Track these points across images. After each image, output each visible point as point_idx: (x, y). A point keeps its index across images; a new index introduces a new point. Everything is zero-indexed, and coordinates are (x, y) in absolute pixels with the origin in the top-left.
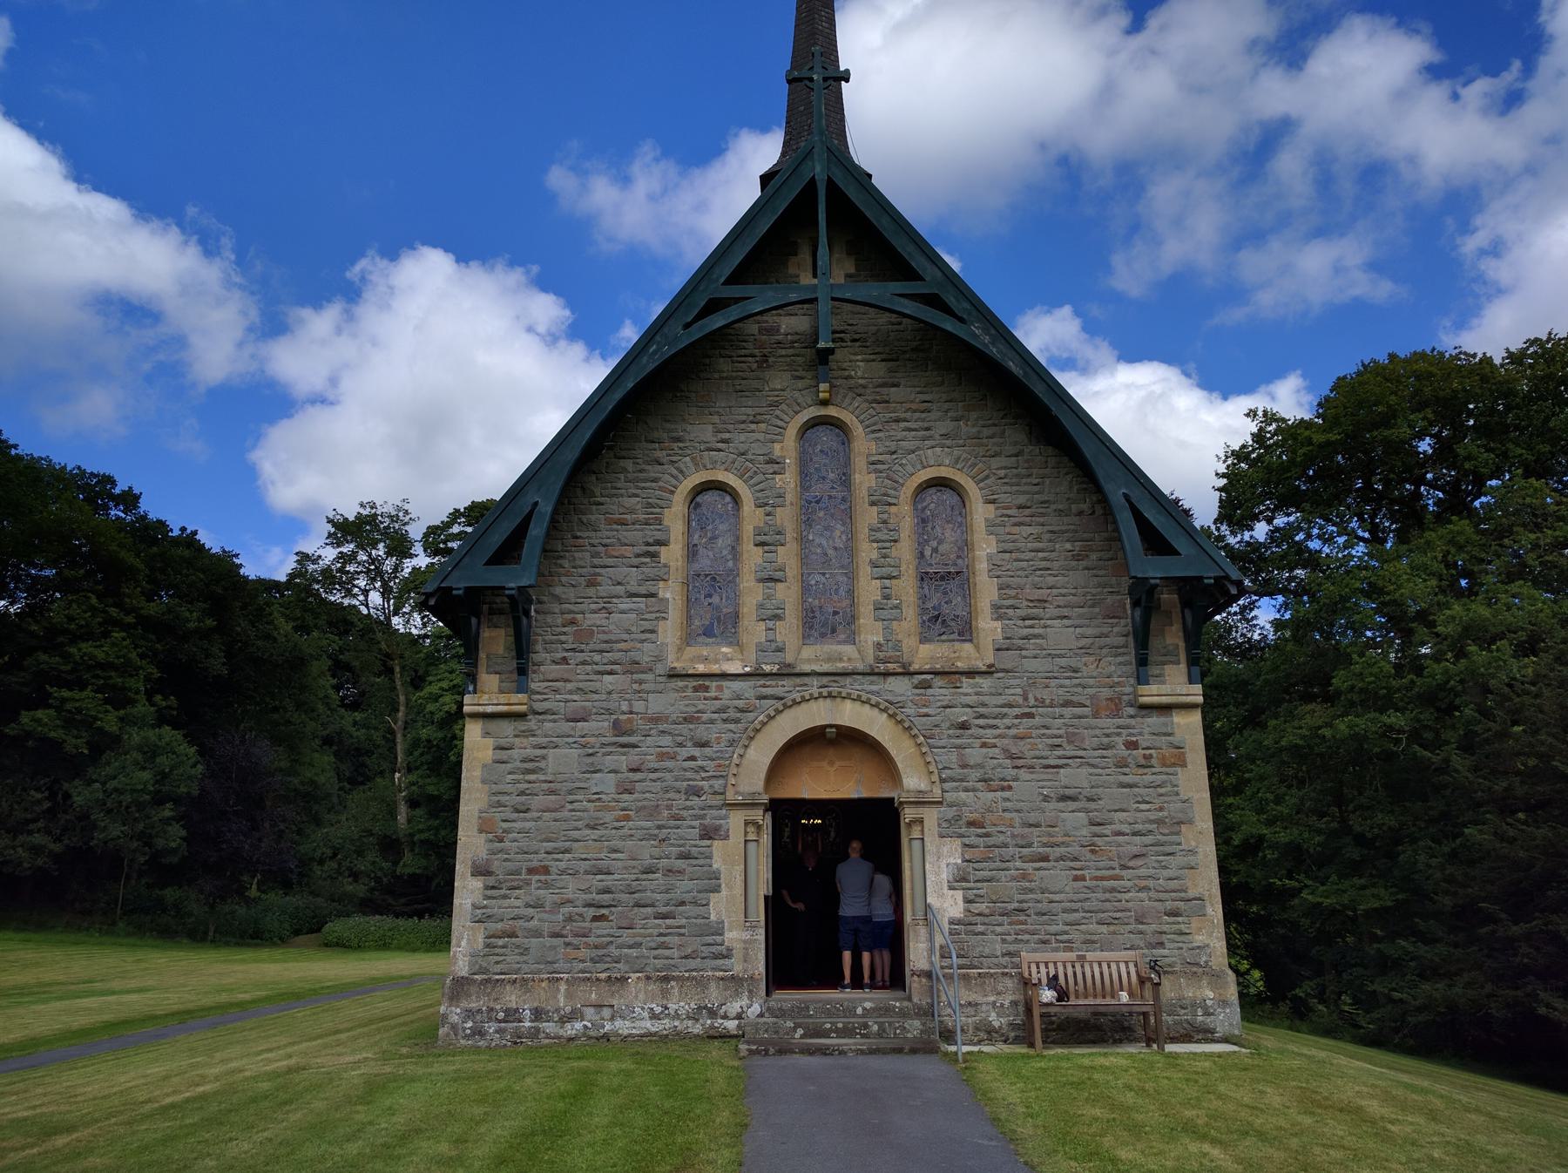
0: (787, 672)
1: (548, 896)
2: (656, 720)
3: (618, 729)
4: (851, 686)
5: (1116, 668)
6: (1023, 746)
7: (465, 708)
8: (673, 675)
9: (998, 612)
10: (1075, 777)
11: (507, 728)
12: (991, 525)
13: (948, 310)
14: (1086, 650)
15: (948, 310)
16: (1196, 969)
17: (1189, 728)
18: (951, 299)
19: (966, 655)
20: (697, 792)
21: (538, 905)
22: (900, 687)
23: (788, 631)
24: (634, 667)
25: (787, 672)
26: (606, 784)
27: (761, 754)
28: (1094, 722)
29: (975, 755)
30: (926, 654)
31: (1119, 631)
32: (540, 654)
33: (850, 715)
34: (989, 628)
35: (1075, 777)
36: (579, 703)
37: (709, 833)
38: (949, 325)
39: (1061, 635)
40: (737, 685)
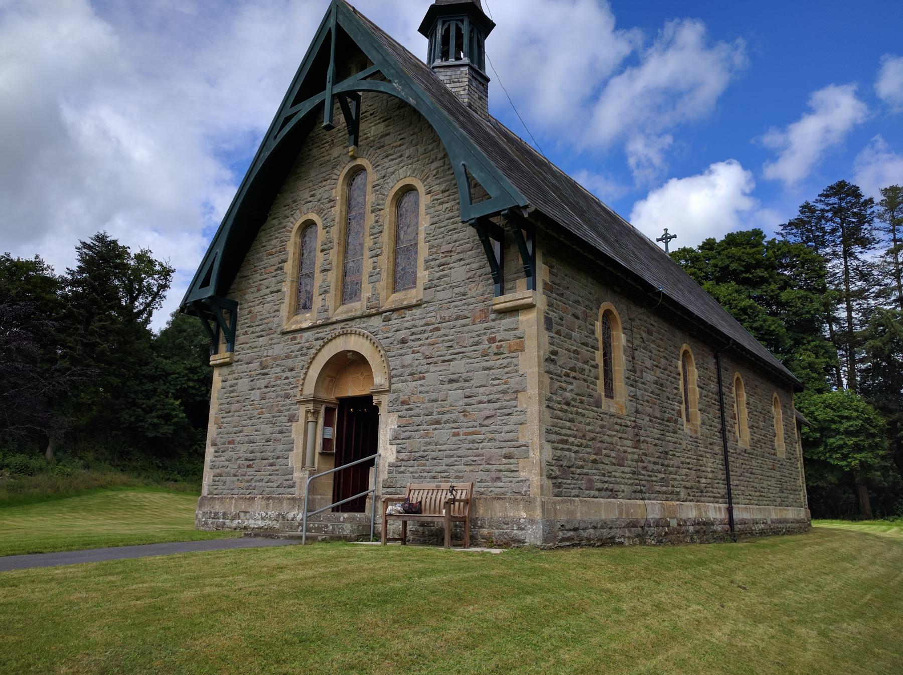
10: (459, 366)
23: (331, 299)
34: (423, 276)
35: (459, 366)
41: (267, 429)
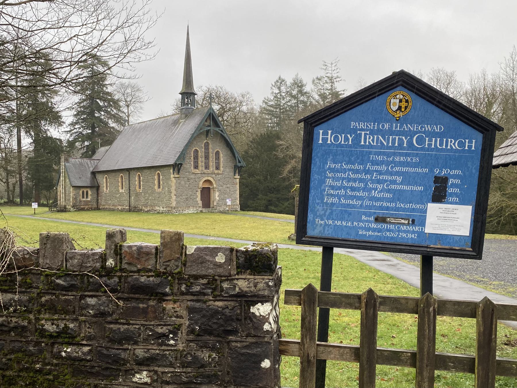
0: (204, 173)
1: (182, 198)
2: (191, 178)
3: (188, 179)
4: (210, 175)
5: (232, 174)
6: (224, 182)
7: (494, 160)
8: (193, 173)
9: (223, 167)
10: (228, 185)
11: (177, 179)
12: (119, 329)
13: (223, 132)
14: (230, 172)
15: (223, 132)
16: (237, 205)
17: (238, 180)
18: (223, 131)
19: (220, 172)
20: (195, 187)
21: (181, 199)
22: (214, 175)
23: (204, 168)
24: (189, 172)
25: (204, 173)
26: (187, 185)
27: (201, 183)
28: (410, 228)
29: (220, 183)
30: (216, 172)
31: (233, 170)
32: (181, 172)
33: (210, 178)
34: (222, 169)
35: (228, 185)
36: (184, 176)
37: (197, 191)
38: (223, 134)
39: (228, 170)
40: (199, 175)
41: (191, 193)
